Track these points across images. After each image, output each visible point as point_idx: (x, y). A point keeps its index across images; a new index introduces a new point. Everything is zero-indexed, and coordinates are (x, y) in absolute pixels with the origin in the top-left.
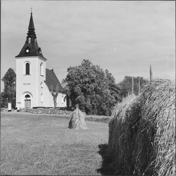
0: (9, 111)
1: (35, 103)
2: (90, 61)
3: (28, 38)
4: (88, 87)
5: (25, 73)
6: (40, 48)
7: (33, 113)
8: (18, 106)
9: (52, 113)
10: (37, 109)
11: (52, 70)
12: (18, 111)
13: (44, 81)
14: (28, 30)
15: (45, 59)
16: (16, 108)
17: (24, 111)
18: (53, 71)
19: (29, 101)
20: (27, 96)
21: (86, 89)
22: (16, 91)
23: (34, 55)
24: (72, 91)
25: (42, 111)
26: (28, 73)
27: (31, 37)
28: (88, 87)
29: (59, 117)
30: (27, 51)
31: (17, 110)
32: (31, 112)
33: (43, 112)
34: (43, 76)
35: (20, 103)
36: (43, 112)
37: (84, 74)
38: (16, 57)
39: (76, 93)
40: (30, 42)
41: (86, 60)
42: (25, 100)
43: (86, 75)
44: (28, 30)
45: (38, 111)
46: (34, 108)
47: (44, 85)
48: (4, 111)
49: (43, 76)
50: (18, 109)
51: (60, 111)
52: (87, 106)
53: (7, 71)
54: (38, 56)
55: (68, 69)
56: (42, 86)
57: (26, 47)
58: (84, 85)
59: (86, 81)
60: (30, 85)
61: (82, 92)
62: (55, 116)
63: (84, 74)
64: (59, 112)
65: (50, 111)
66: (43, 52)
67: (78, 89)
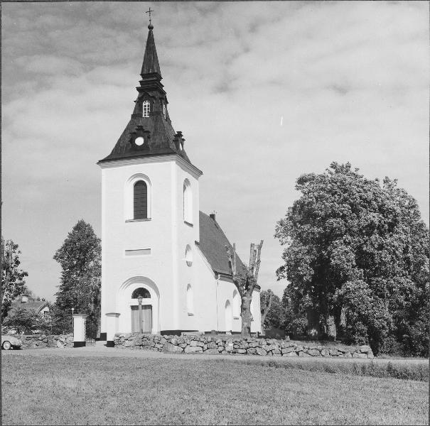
0: (77, 344)
1: (165, 316)
2: (357, 169)
3: (139, 102)
4: (379, 245)
5: (131, 215)
6: (180, 134)
7: (167, 351)
8: (108, 326)
9: (240, 351)
10: (179, 335)
11: (212, 216)
12: (111, 344)
13: (196, 243)
14: (141, 79)
15: (198, 173)
16: (104, 336)
17: (131, 343)
18: (214, 219)
19: (148, 310)
20: (141, 293)
21: (372, 255)
22: (98, 292)
23: (161, 152)
24: (322, 265)
25: (202, 345)
26: (141, 211)
27: (151, 99)
28: (381, 247)
29: (287, 366)
30: (139, 141)
31: (105, 342)
32: (158, 346)
33: (206, 347)
34: (191, 225)
35: (118, 315)
36: (206, 347)
37: (361, 197)
38: (101, 162)
39: (338, 268)
40: (146, 114)
41: (340, 164)
42: (134, 308)
43: (369, 203)
44: (141, 79)
45: (184, 346)
46: (163, 333)
47: (197, 256)
48: (59, 344)
49: (191, 225)
50: (110, 338)
51: (271, 341)
52: (377, 323)
53: (71, 230)
54: (174, 157)
55: (302, 181)
56: (190, 258)
57: (135, 129)
58: (366, 238)
59: (372, 222)
60: (150, 253)
61: (360, 265)
62: (270, 364)
63: (361, 197)
64: (269, 348)
65: (231, 345)
66: (187, 147)
67: (342, 254)
